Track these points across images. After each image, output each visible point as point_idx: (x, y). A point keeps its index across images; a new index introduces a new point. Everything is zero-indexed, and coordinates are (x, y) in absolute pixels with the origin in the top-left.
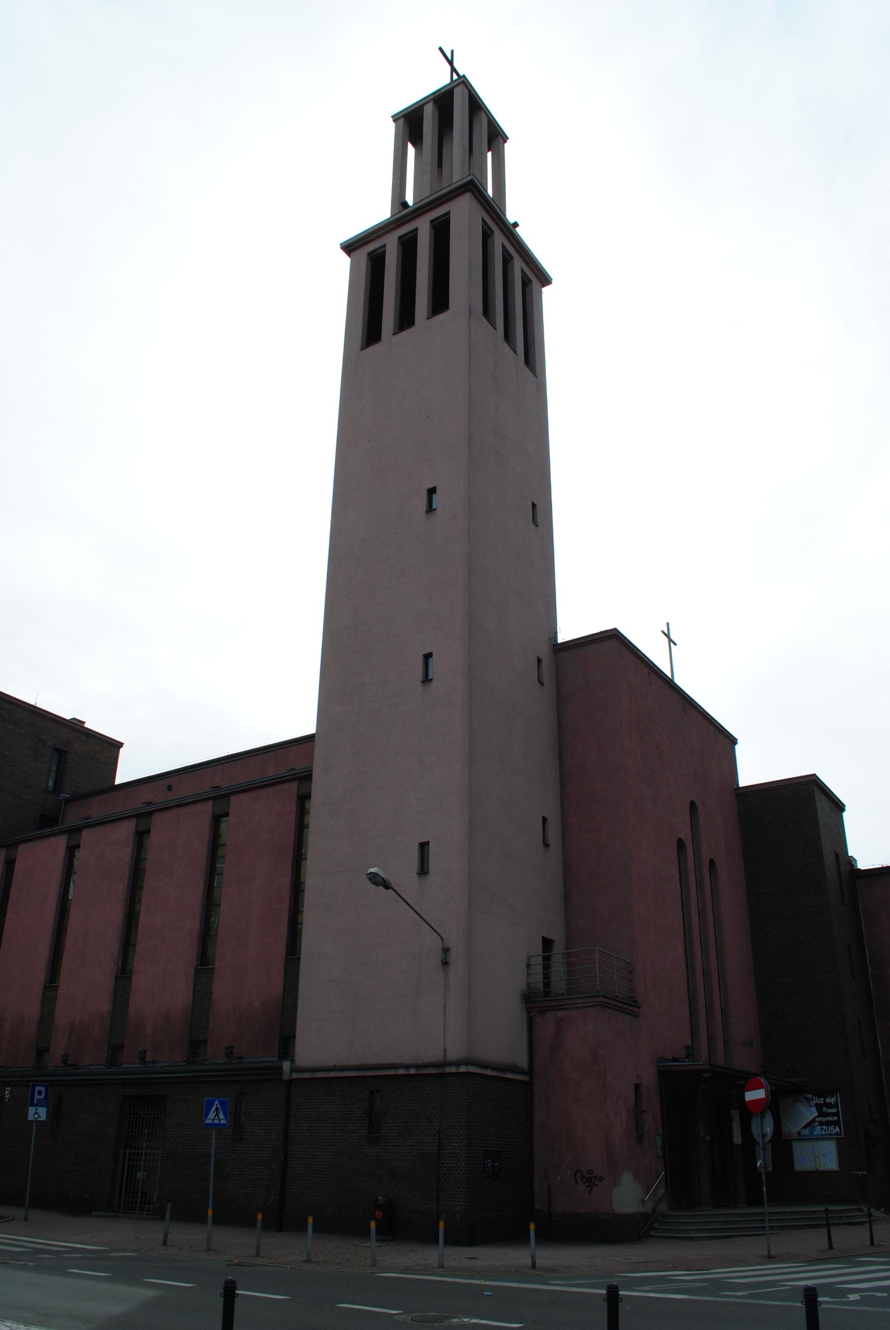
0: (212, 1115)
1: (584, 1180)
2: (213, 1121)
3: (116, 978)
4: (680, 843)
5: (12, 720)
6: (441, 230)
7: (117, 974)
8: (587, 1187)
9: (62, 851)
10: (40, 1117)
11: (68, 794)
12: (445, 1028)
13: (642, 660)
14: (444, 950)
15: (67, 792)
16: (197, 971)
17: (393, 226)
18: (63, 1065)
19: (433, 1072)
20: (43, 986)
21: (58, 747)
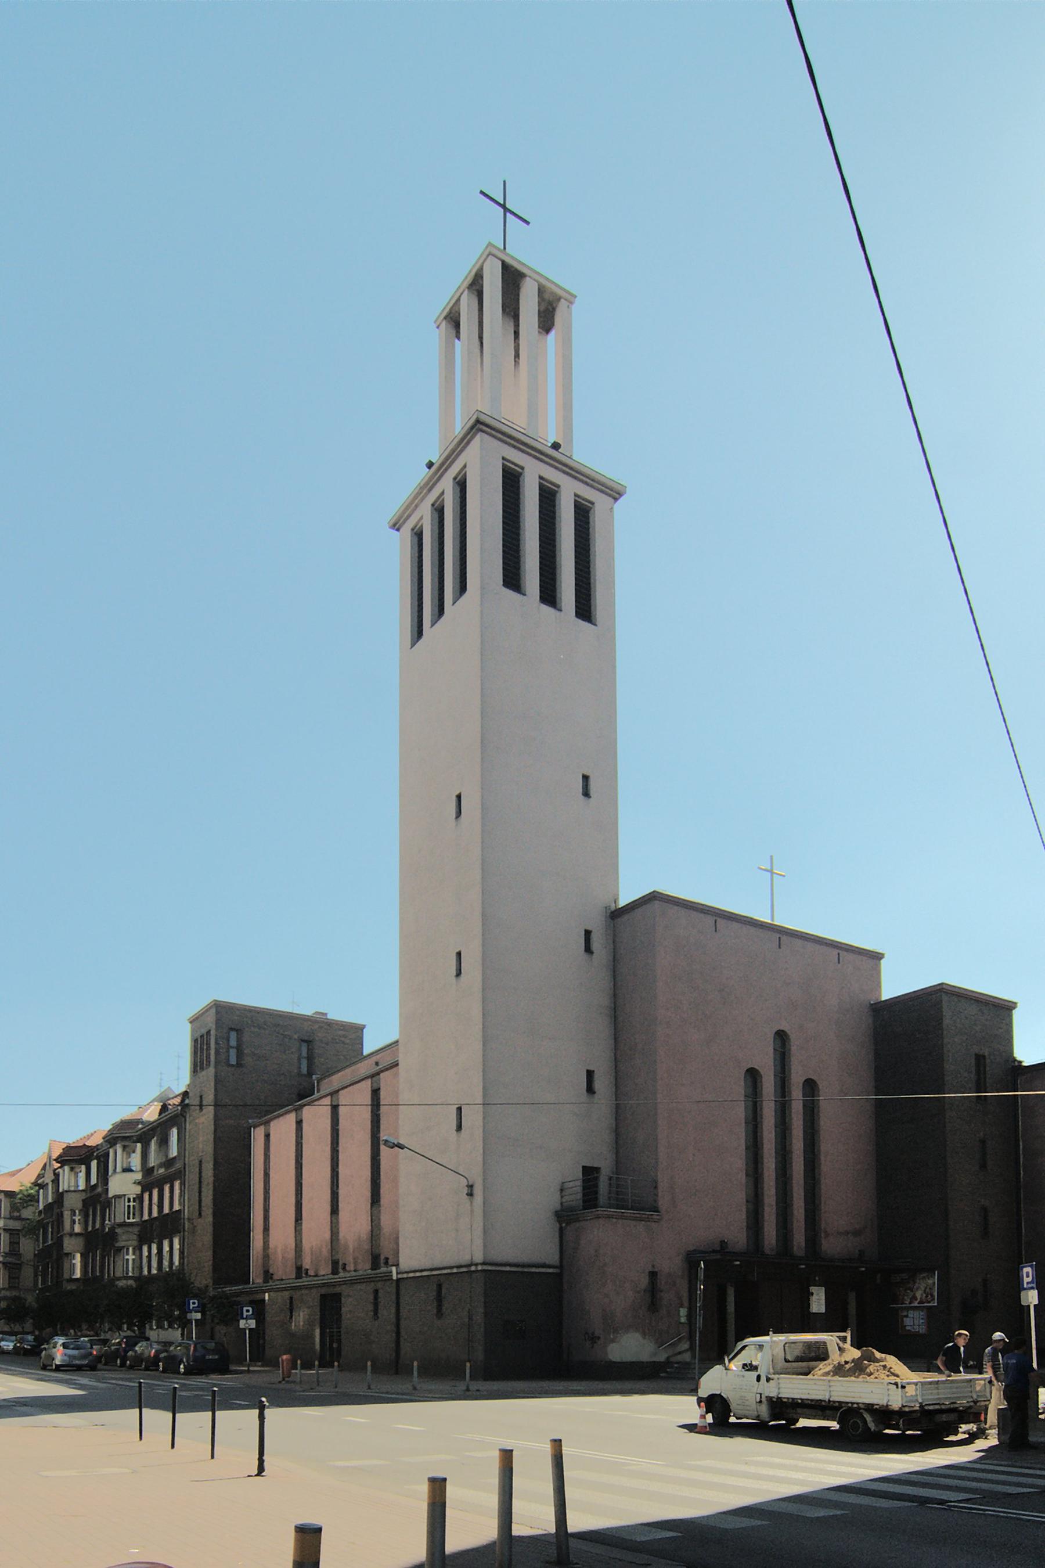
4: (753, 1075)
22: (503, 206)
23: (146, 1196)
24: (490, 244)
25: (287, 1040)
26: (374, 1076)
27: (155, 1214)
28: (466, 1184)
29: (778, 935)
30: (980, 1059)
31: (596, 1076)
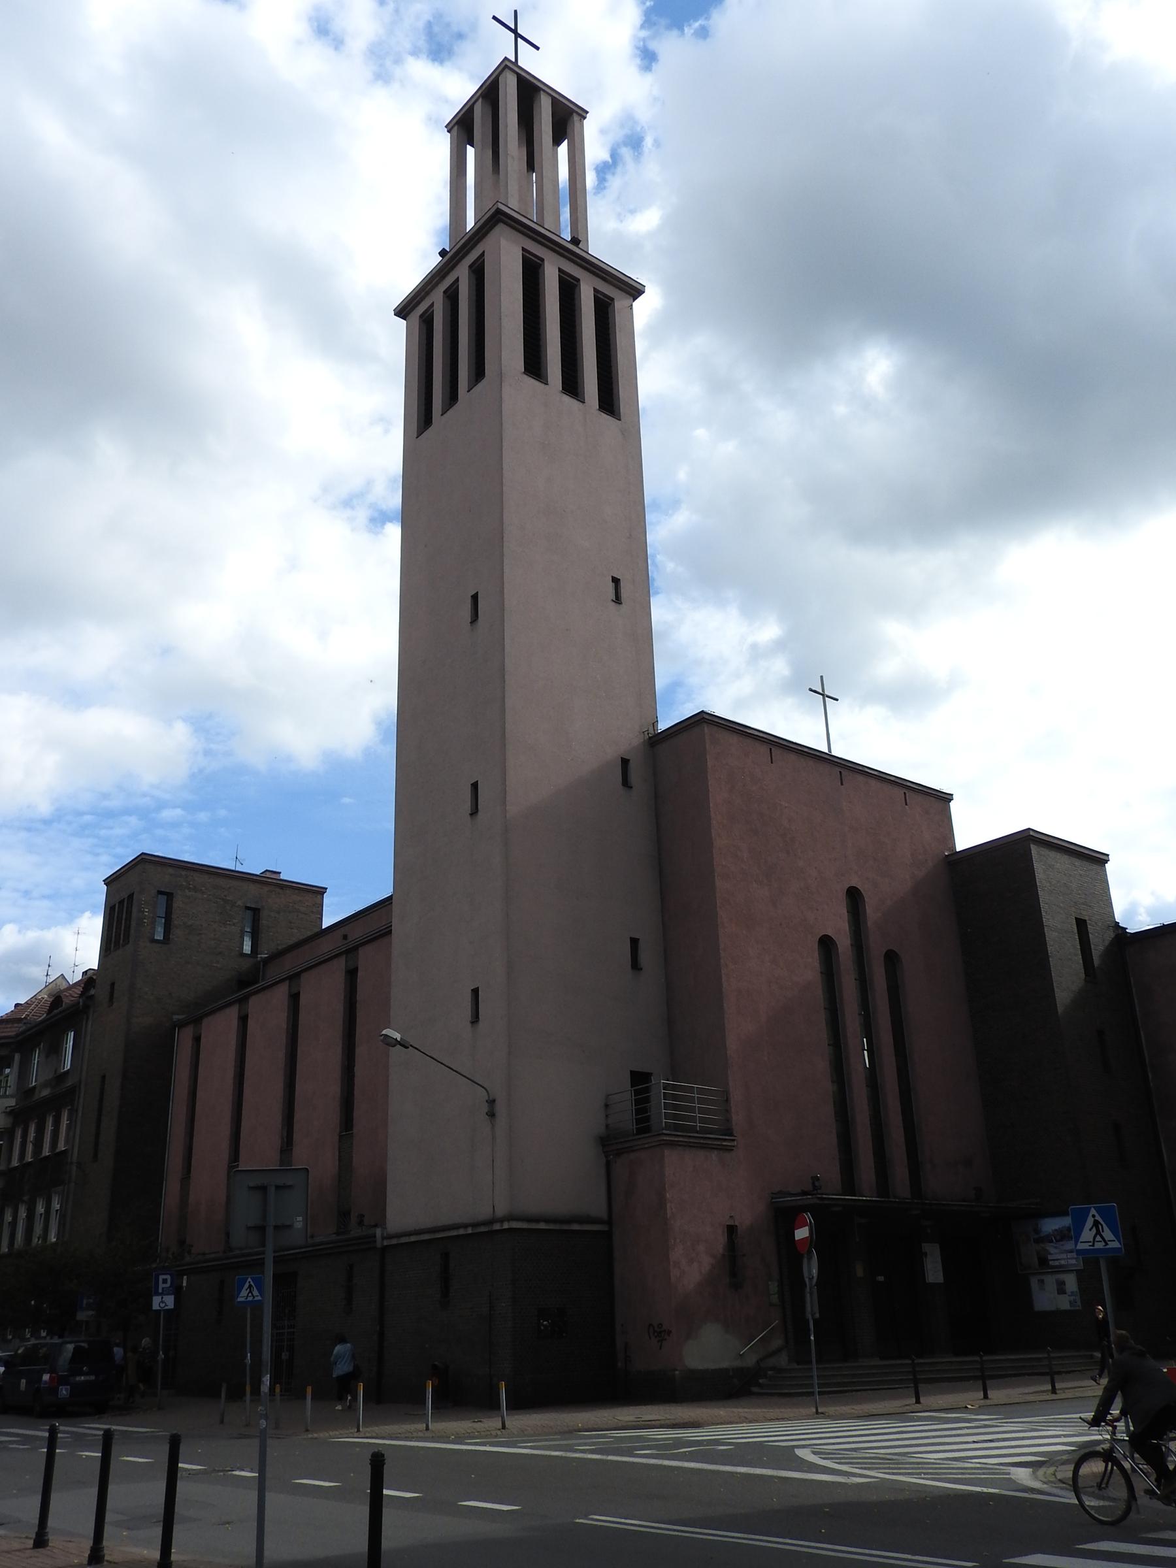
0: (244, 1293)
1: (656, 1334)
3: (281, 1151)
4: (826, 944)
5: (191, 886)
6: (478, 272)
7: (281, 1148)
8: (658, 1341)
9: (235, 1023)
12: (493, 1183)
13: (753, 736)
15: (266, 952)
16: (341, 1137)
20: (226, 1166)
21: (248, 905)
23: (19, 1134)
24: (506, 58)
25: (228, 908)
27: (29, 1158)
28: (487, 1098)
29: (839, 769)
30: (1081, 924)
31: (642, 945)
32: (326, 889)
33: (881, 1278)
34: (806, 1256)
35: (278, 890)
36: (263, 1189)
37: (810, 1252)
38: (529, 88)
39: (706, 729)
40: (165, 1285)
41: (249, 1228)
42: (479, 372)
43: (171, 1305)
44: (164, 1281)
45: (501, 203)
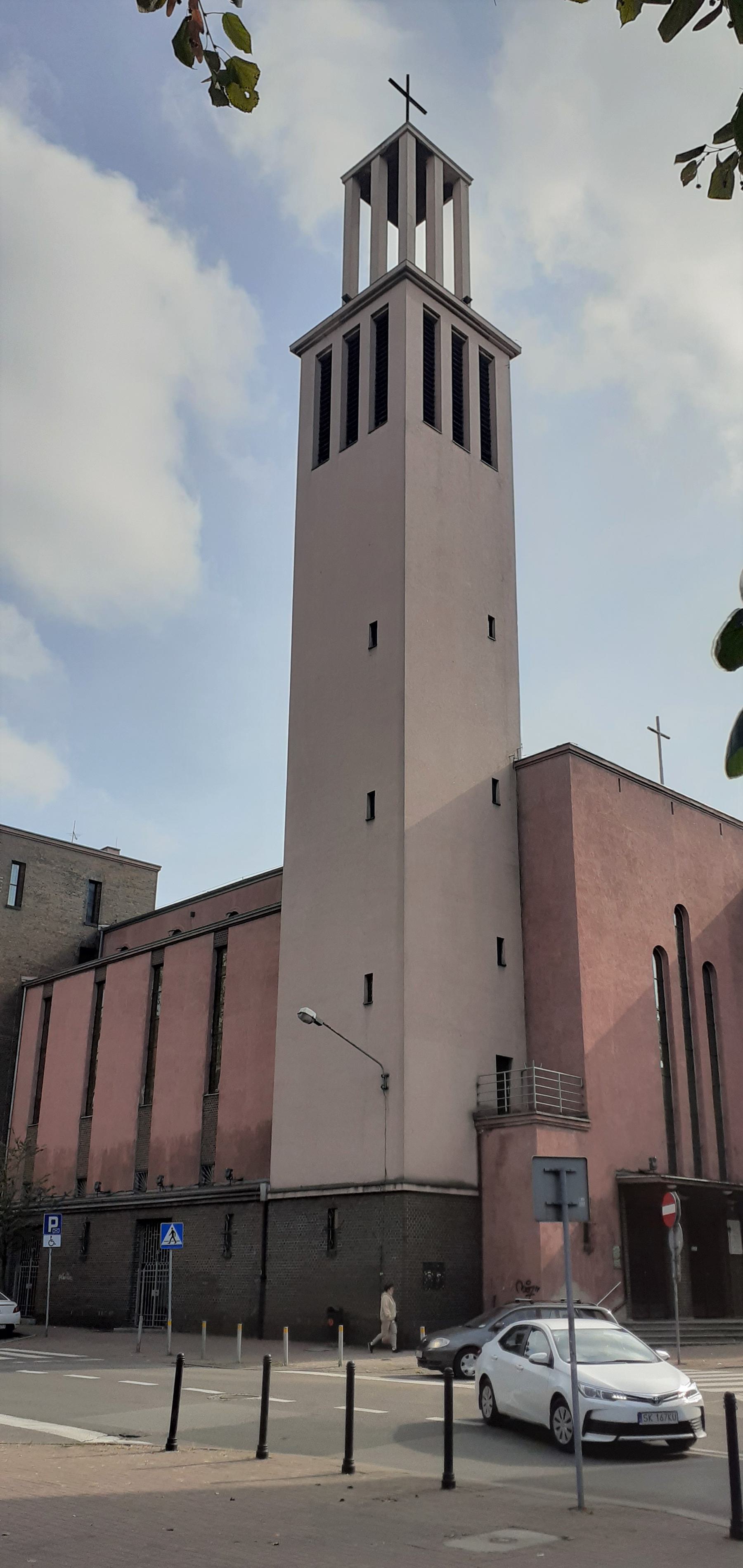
0: (168, 1237)
2: (170, 1243)
3: (140, 1108)
6: (381, 322)
7: (140, 1105)
9: (90, 988)
10: (55, 1244)
11: (107, 924)
14: (383, 1076)
15: (106, 922)
16: (205, 1098)
17: (338, 322)
18: (96, 1193)
19: (376, 1191)
20: (79, 1118)
21: (92, 879)
22: (409, 99)
25: (74, 880)
26: (221, 930)
28: (382, 1073)
32: (160, 867)
33: (695, 1249)
34: (672, 1229)
35: (118, 865)
36: (556, 1173)
37: (675, 1227)
38: (425, 152)
39: (571, 759)
40: (53, 1226)
41: (547, 1205)
42: (380, 416)
43: (58, 1245)
44: (53, 1222)
45: (409, 261)
